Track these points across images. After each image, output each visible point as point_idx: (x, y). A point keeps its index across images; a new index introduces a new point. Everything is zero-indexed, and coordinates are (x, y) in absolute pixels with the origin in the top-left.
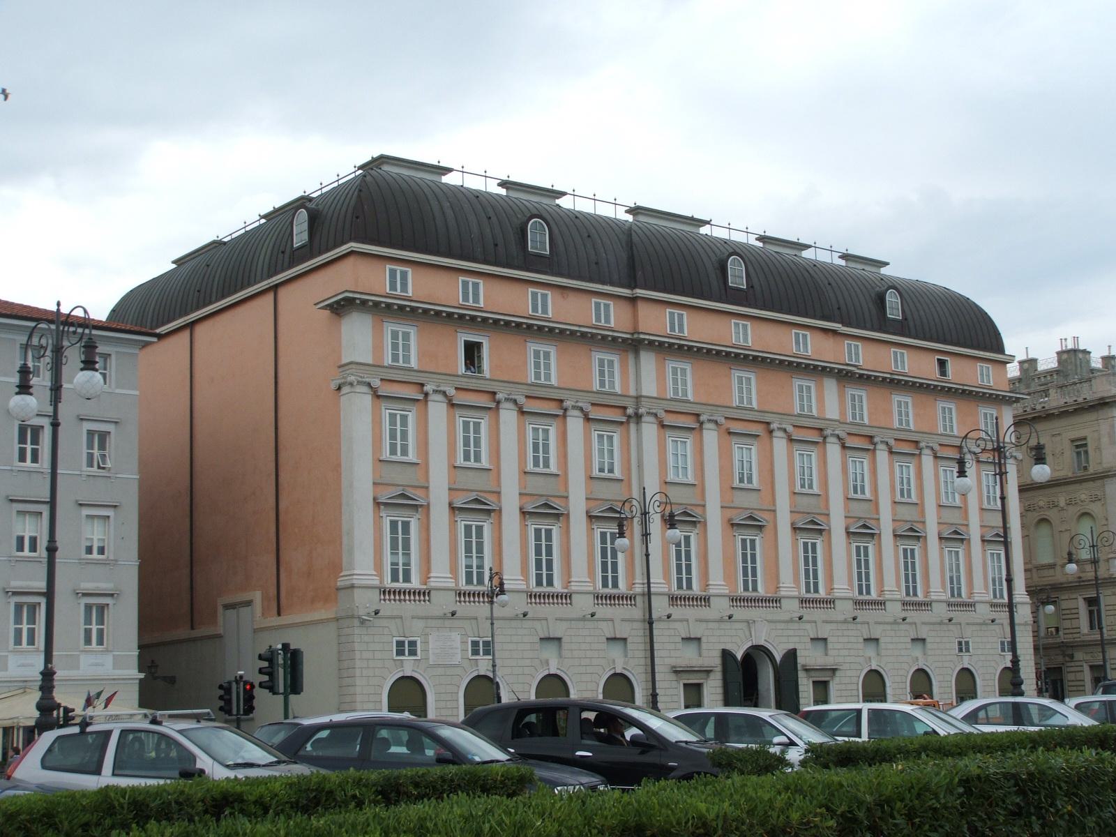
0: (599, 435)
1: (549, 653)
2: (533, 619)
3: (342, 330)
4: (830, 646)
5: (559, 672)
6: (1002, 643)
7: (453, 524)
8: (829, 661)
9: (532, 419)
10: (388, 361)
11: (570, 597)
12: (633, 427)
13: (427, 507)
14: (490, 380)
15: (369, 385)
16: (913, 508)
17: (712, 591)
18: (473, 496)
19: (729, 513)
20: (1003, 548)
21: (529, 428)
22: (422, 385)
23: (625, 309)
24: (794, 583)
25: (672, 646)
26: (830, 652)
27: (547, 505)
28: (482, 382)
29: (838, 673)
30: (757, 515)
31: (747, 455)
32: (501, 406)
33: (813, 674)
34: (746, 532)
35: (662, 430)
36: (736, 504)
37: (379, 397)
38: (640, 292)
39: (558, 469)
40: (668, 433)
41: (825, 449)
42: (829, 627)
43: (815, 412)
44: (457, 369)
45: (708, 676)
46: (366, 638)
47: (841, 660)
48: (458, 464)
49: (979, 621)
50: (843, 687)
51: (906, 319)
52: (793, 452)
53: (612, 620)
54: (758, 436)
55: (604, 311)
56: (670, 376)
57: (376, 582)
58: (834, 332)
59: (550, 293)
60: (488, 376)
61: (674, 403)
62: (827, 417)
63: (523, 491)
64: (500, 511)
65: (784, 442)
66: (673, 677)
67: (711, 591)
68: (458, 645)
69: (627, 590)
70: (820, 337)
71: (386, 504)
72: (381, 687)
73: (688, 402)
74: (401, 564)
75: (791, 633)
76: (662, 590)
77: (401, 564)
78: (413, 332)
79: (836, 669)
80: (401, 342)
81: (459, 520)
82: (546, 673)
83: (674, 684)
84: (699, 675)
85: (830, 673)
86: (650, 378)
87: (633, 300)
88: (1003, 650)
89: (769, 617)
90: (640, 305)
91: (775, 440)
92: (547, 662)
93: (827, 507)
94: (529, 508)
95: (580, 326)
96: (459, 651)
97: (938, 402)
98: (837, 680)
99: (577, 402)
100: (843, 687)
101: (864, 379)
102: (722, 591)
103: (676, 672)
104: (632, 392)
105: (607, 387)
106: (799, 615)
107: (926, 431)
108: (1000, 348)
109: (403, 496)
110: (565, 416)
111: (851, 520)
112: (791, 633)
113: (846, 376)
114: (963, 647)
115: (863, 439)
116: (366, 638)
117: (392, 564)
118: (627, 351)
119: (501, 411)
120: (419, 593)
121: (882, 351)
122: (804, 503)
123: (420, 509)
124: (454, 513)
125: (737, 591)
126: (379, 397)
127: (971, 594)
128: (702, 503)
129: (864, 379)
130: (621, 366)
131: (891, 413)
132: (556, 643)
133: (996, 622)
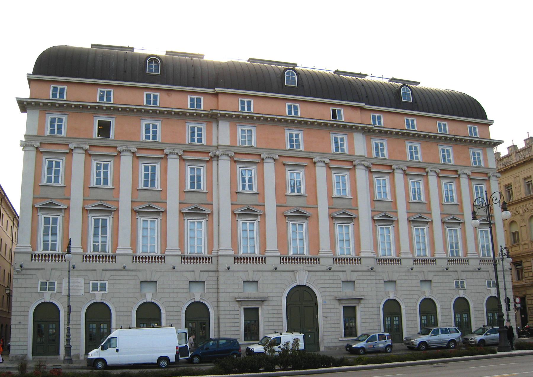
0: (191, 168)
1: (390, 288)
2: (376, 272)
3: (355, 141)
4: (356, 285)
5: (153, 301)
6: (489, 282)
7: (410, 229)
8: (356, 294)
9: (377, 175)
10: (374, 156)
11: (400, 260)
12: (214, 163)
13: (464, 223)
14: (206, 146)
15: (467, 174)
16: (423, 205)
17: (362, 255)
18: (383, 214)
19: (283, 209)
20: (488, 227)
21: (188, 169)
22: (352, 162)
23: (212, 99)
24: (374, 250)
25: (236, 286)
26: (356, 289)
27: (298, 211)
28: (110, 142)
29: (362, 301)
30: (301, 210)
31: (296, 177)
32: (429, 174)
33: (343, 302)
34: (98, 214)
35: (406, 176)
36: (288, 204)
37: (471, 179)
38: (218, 90)
39: (458, 202)
40: (409, 178)
41: (355, 172)
42: (356, 274)
43: (346, 151)
44: (186, 140)
45: (360, 302)
46: (20, 281)
47: (365, 293)
48: (444, 203)
49: (471, 270)
50: (367, 309)
51: (416, 102)
52: (441, 183)
53: (193, 271)
54: (306, 166)
55: (320, 112)
56: (374, 147)
57: (30, 250)
58: (361, 108)
59: (342, 109)
60: (113, 138)
61: (242, 149)
62: (356, 154)
63: (443, 213)
64: (432, 221)
65: (324, 169)
66: (237, 304)
67: (166, 253)
68: (83, 284)
69: (431, 256)
70: (349, 111)
71: (239, 214)
72: (29, 307)
73: (253, 147)
74: (100, 242)
75: (327, 278)
76: (79, 251)
77: (100, 242)
78: (253, 130)
79: (361, 299)
80: (446, 154)
81: (239, 220)
82: (388, 298)
83: (337, 306)
84: (354, 301)
85: (357, 301)
86: (223, 134)
87: (216, 94)
88: (489, 286)
89: (310, 269)
90: (220, 96)
91: (317, 168)
92: (424, 292)
93: (357, 205)
94: (446, 220)
95: (172, 108)
96: (83, 288)
97: (187, 124)
98: (362, 305)
99: (174, 150)
100: (367, 309)
101: (383, 133)
102: (275, 254)
103: (238, 301)
104: (214, 144)
105: (196, 141)
106: (479, 267)
107: (431, 162)
108: (484, 116)
109: (453, 219)
110: (393, 173)
111: (445, 216)
112: (327, 278)
113: (368, 132)
114: (460, 285)
115: (348, 163)
116: (20, 281)
117: (94, 242)
118: (212, 122)
119: (395, 174)
120: (396, 260)
121: (174, 96)
122: (416, 208)
123: (259, 217)
124: (375, 222)
125: (288, 254)
126: (406, 175)
127: (466, 254)
128: (262, 204)
129: (383, 133)
130: (207, 130)
131: (405, 152)
132: (255, 284)
133: (449, 269)
